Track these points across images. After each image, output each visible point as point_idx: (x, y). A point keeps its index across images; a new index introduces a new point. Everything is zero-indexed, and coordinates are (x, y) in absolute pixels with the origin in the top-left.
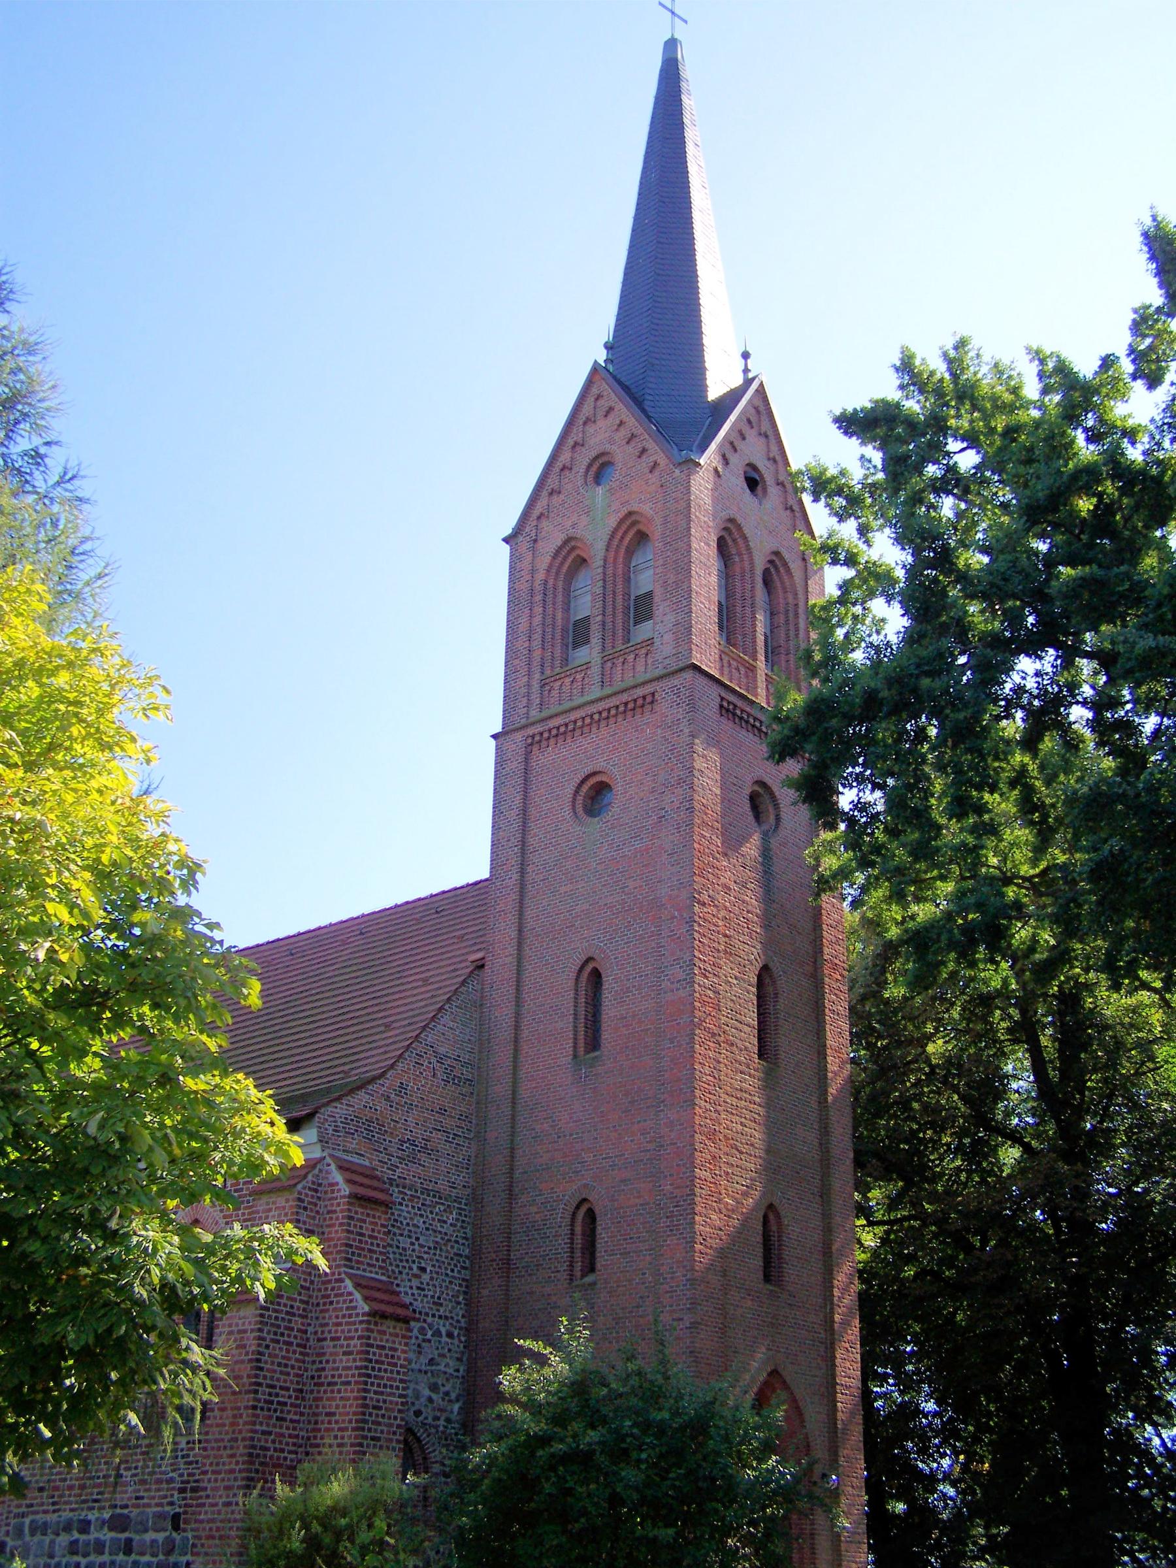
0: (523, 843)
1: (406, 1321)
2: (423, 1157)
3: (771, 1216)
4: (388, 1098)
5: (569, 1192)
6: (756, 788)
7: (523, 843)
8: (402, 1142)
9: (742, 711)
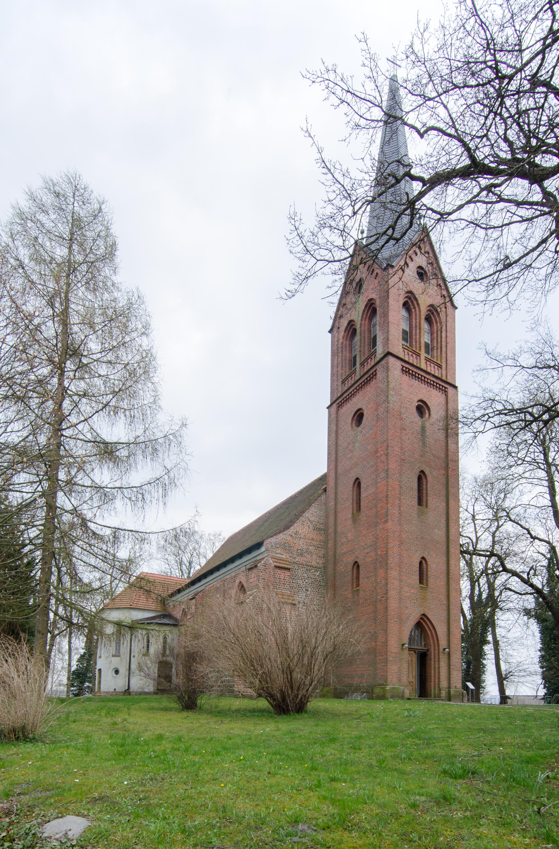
0: (337, 443)
1: (256, 566)
2: (306, 554)
3: (424, 562)
4: (291, 536)
5: (351, 560)
6: (420, 403)
7: (337, 443)
8: (298, 550)
9: (413, 371)
